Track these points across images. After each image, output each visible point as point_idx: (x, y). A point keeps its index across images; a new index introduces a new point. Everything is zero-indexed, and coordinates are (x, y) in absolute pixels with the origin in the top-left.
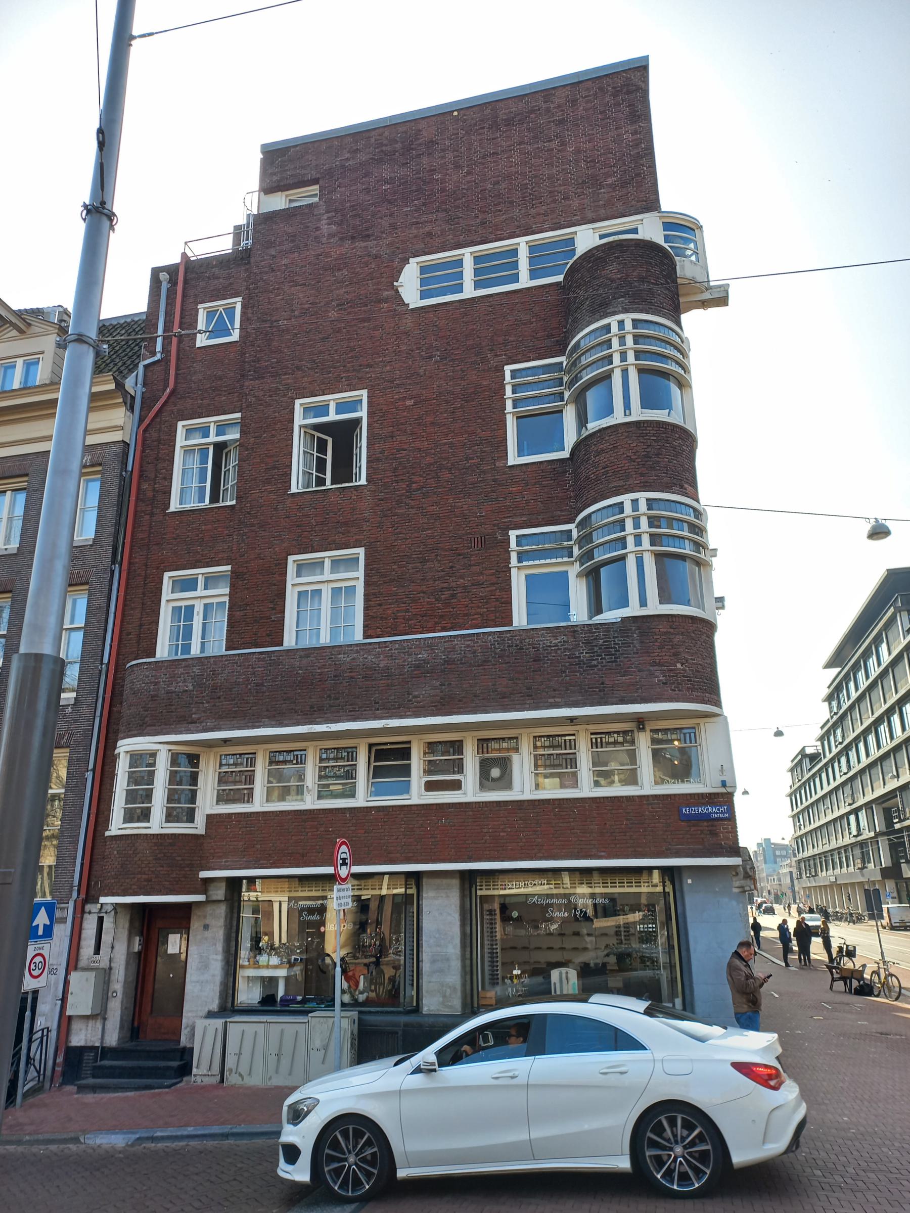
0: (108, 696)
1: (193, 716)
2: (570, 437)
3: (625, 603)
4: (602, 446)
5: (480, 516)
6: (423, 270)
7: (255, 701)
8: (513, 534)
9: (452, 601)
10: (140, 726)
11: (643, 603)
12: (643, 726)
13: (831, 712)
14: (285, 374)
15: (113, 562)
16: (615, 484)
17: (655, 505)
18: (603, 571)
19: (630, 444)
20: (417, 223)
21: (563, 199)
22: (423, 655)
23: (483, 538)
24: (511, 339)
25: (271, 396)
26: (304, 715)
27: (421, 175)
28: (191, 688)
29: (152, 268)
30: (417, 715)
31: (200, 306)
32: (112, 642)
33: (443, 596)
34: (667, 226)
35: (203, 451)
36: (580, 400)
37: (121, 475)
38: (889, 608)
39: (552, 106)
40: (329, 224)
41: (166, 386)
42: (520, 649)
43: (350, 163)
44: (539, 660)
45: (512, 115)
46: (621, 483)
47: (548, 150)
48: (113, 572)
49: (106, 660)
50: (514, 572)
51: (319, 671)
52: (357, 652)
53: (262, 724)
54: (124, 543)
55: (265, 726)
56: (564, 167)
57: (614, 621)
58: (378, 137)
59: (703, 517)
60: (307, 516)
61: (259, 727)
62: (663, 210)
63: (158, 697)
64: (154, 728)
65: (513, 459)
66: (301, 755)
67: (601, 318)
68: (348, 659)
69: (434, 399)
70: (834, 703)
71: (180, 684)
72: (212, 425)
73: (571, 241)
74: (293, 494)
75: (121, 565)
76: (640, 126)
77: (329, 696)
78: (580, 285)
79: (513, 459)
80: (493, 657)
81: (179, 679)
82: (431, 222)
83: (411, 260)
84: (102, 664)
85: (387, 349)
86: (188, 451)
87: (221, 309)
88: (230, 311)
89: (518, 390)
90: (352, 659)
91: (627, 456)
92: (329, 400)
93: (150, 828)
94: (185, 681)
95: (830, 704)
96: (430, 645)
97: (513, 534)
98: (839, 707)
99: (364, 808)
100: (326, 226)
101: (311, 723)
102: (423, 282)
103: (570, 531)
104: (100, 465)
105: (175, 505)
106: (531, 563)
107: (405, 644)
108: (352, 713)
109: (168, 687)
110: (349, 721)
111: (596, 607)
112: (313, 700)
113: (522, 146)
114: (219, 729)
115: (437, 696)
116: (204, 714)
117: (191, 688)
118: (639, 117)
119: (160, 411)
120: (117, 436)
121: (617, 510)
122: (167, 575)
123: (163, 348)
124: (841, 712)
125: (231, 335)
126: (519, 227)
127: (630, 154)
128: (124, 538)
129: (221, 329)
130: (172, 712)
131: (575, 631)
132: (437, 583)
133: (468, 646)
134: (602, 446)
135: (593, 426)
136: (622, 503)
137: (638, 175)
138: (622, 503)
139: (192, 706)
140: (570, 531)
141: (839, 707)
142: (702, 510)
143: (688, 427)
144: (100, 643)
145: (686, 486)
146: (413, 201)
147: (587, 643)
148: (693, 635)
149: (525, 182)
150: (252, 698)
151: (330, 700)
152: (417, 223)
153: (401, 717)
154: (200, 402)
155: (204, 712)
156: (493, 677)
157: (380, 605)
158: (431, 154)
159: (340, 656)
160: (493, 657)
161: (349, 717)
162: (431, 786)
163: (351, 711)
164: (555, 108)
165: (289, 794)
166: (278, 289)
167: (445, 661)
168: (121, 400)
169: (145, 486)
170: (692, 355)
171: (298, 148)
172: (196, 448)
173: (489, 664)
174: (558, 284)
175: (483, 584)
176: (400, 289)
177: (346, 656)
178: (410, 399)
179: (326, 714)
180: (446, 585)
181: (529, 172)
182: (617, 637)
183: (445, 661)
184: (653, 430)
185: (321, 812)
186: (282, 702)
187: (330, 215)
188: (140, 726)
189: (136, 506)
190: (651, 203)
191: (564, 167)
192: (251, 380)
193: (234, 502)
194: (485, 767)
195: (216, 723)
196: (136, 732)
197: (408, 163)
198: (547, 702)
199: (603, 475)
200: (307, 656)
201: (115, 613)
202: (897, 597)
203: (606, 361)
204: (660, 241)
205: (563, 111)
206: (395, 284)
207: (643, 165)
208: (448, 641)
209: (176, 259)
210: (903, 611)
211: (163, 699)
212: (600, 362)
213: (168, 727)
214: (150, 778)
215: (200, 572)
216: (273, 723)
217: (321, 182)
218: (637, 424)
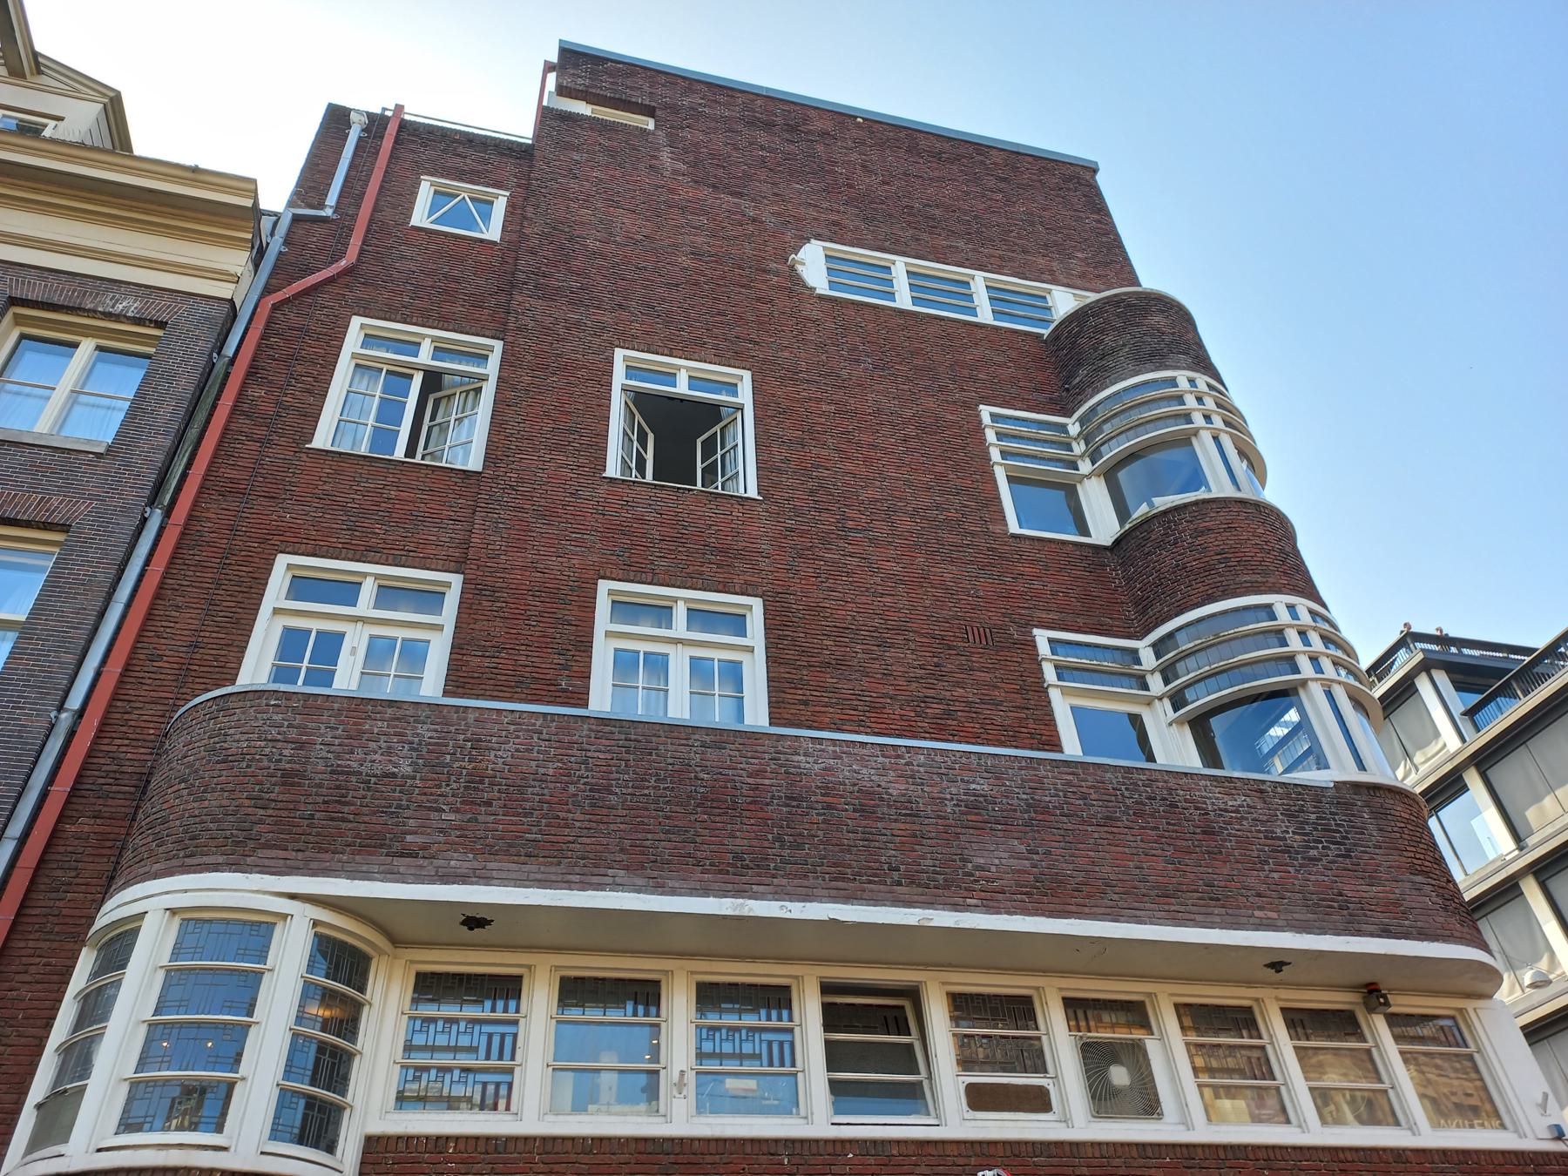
0: (62, 788)
1: (409, 838)
7: (586, 824)
10: (237, 843)
15: (152, 502)
16: (1248, 578)
18: (1215, 722)
22: (982, 786)
26: (720, 872)
28: (406, 769)
29: (330, 105)
30: (990, 907)
32: (104, 662)
35: (400, 376)
37: (210, 355)
41: (342, 255)
42: (1170, 806)
44: (1214, 833)
48: (144, 520)
49: (75, 701)
51: (750, 780)
52: (836, 757)
53: (610, 880)
54: (184, 476)
55: (616, 886)
57: (1324, 785)
60: (642, 520)
61: (599, 887)
63: (304, 777)
64: (281, 854)
66: (503, 1036)
67: (1167, 368)
68: (816, 767)
71: (377, 757)
72: (427, 342)
75: (168, 513)
77: (779, 839)
81: (373, 745)
82: (839, 212)
83: (813, 241)
84: (60, 708)
86: (362, 367)
90: (825, 769)
93: (225, 1149)
94: (389, 752)
96: (995, 770)
99: (826, 1141)
101: (739, 893)
104: (161, 325)
105: (322, 439)
107: (938, 758)
108: (840, 884)
109: (338, 757)
110: (834, 899)
112: (738, 842)
114: (486, 880)
115: (1025, 872)
116: (441, 838)
117: (406, 769)
119: (316, 288)
120: (224, 290)
122: (282, 561)
123: (338, 202)
128: (189, 465)
130: (344, 820)
131: (1262, 791)
133: (1069, 784)
135: (1141, 511)
139: (408, 813)
144: (70, 659)
146: (809, 182)
147: (1290, 815)
150: (578, 816)
151: (782, 847)
153: (956, 907)
155: (442, 830)
156: (1134, 851)
157: (805, 703)
159: (796, 758)
161: (833, 892)
162: (980, 1098)
163: (836, 879)
165: (594, 1099)
167: (1029, 806)
168: (249, 236)
169: (256, 392)
172: (385, 368)
173: (1119, 824)
176: (799, 268)
177: (811, 760)
179: (774, 876)
180: (931, 693)
182: (1337, 814)
183: (1029, 806)
185: (713, 1145)
186: (663, 836)
188: (237, 843)
189: (230, 420)
194: (1096, 1058)
195: (476, 864)
196: (221, 859)
198: (1252, 916)
200: (718, 745)
201: (128, 605)
208: (1027, 768)
209: (378, 111)
211: (319, 786)
213: (327, 856)
214: (245, 991)
215: (370, 574)
216: (639, 881)
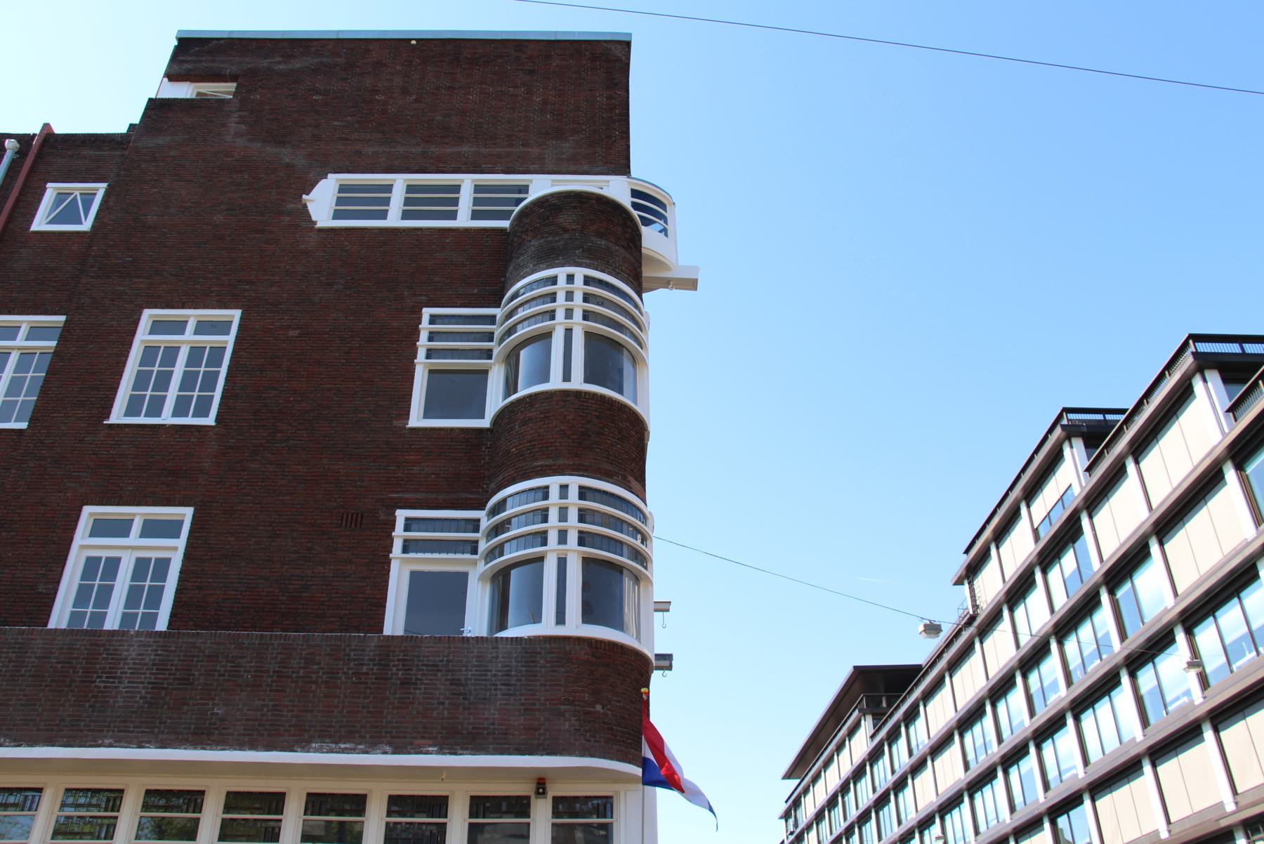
2: (495, 401)
3: (536, 618)
4: (530, 414)
5: (361, 487)
6: (343, 188)
8: (401, 515)
9: (303, 595)
11: (560, 619)
12: (544, 789)
13: (787, 831)
14: (139, 277)
17: (588, 495)
19: (566, 416)
20: (346, 139)
21: (522, 145)
23: (359, 515)
24: (437, 279)
25: (112, 300)
27: (361, 93)
31: (49, 185)
33: (290, 587)
34: (635, 193)
36: (512, 360)
38: (854, 710)
39: (523, 56)
40: (238, 123)
43: (281, 67)
45: (477, 56)
46: (551, 462)
47: (512, 95)
50: (395, 567)
56: (527, 114)
58: (320, 48)
59: (649, 522)
62: (632, 176)
65: (417, 419)
69: (326, 333)
70: (791, 821)
73: (524, 189)
74: (111, 425)
76: (615, 93)
78: (527, 231)
79: (417, 419)
80: (344, 673)
85: (278, 267)
87: (77, 193)
88: (88, 198)
89: (436, 338)
91: (561, 430)
92: (135, 515)
95: (786, 821)
97: (401, 515)
98: (796, 825)
100: (234, 125)
102: (340, 201)
103: (478, 521)
106: (420, 555)
111: (500, 616)
113: (482, 86)
118: (616, 85)
121: (540, 494)
124: (798, 830)
125: (81, 223)
126: (465, 164)
127: (602, 117)
129: (70, 214)
132: (286, 567)
134: (530, 414)
135: (522, 392)
136: (547, 487)
137: (610, 137)
138: (547, 487)
140: (478, 521)
141: (796, 825)
142: (648, 514)
143: (638, 409)
145: (630, 478)
148: (621, 668)
149: (480, 120)
152: (346, 139)
154: (15, 295)
158: (377, 75)
160: (344, 673)
164: (526, 58)
166: (156, 180)
170: (650, 333)
171: (222, 42)
174: (501, 231)
175: (349, 577)
178: (294, 329)
181: (487, 112)
184: (596, 404)
187: (243, 113)
190: (621, 166)
191: (527, 114)
192: (92, 277)
193: (23, 425)
197: (348, 79)
199: (528, 450)
202: (862, 698)
203: (548, 316)
204: (628, 206)
205: (534, 62)
206: (304, 196)
207: (615, 130)
209: (35, 129)
210: (868, 714)
212: (540, 317)
217: (239, 80)
218: (578, 394)
